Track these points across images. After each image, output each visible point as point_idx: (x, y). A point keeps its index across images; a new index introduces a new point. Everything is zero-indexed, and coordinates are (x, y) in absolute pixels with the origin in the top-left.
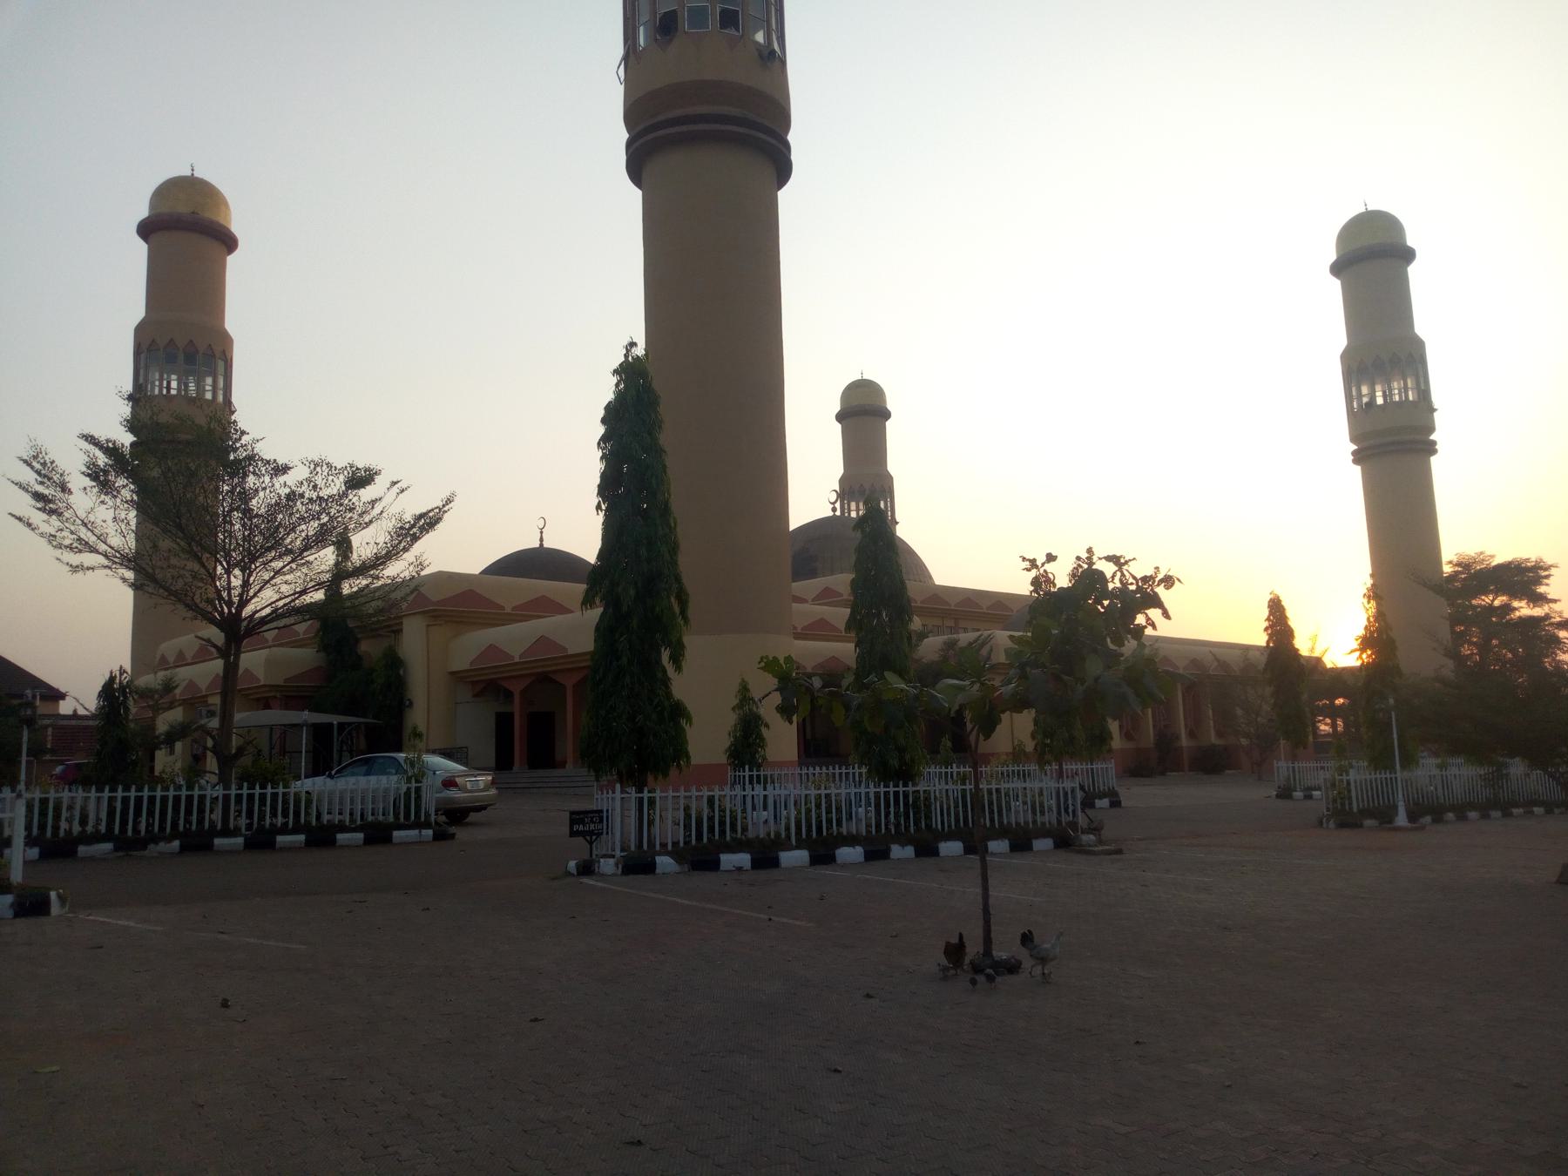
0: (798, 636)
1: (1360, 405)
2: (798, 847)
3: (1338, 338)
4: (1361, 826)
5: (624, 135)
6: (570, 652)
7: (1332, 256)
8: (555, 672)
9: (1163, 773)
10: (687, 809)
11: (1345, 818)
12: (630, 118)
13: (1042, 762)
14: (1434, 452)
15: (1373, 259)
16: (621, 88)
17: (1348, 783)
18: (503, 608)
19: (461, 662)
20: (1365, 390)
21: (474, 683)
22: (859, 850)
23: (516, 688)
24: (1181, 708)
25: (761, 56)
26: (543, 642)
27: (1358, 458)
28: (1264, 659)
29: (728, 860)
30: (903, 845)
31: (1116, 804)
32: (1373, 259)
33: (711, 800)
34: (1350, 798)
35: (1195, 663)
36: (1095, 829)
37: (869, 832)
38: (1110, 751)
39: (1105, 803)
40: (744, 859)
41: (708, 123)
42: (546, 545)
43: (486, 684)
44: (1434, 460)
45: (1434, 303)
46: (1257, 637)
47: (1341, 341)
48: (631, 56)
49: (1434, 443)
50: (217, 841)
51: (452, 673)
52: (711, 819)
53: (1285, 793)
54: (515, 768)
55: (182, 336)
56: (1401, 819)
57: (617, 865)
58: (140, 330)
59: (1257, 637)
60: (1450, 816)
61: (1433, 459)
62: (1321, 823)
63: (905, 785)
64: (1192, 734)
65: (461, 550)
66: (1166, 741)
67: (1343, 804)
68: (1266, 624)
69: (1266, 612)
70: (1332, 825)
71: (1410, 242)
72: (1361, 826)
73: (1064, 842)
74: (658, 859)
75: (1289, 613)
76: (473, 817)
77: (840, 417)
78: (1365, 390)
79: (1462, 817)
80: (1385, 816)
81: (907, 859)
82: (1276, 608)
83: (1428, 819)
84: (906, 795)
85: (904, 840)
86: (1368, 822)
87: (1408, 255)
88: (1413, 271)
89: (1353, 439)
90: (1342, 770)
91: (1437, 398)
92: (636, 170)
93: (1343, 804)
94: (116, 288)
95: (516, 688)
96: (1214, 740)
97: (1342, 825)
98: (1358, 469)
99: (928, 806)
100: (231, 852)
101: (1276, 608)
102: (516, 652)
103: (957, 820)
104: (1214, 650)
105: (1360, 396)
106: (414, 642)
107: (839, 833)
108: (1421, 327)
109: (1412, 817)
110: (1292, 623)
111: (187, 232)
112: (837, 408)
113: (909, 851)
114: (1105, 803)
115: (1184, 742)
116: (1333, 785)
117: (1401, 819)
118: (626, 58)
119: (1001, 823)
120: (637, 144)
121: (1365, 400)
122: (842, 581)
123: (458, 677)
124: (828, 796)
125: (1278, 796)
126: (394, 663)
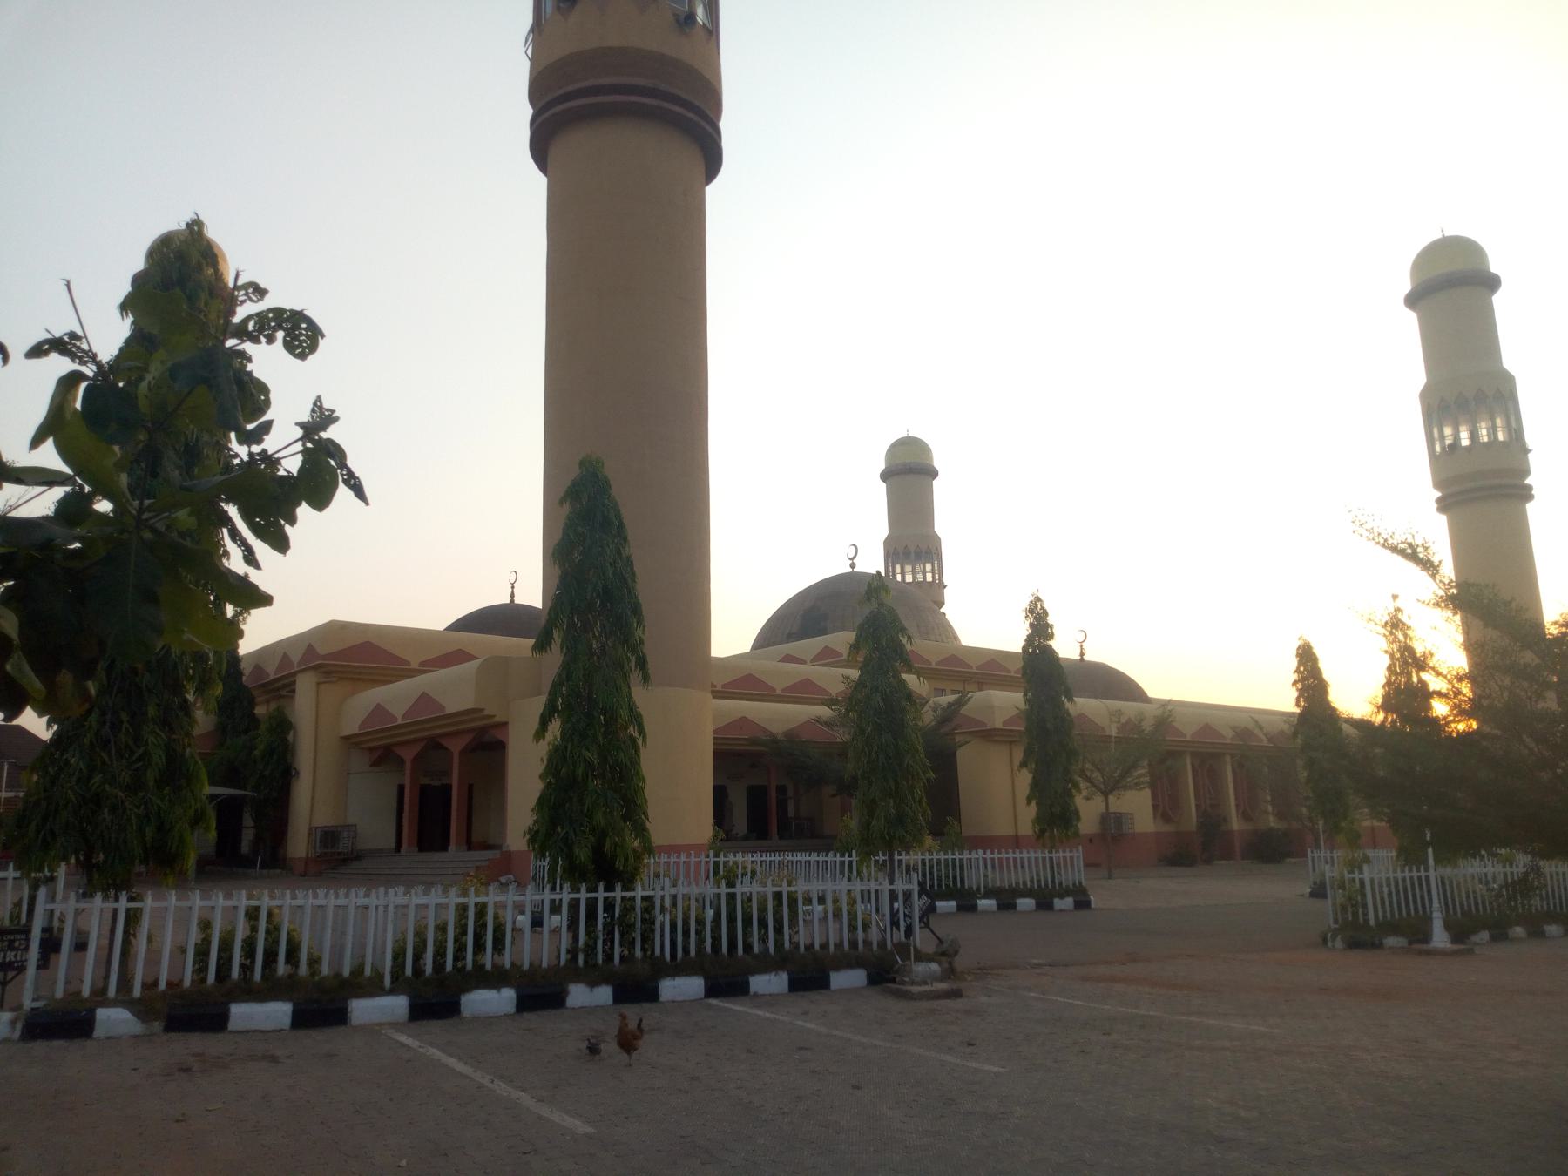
0: (717, 694)
1: (1443, 447)
2: (392, 992)
3: (1418, 376)
4: (1380, 946)
5: (528, 112)
6: (448, 711)
7: (1406, 286)
8: (441, 736)
9: (1208, 861)
10: (206, 926)
11: (1359, 935)
12: (534, 96)
13: (866, 855)
14: (1529, 497)
15: (1453, 287)
16: (527, 64)
17: (1362, 882)
18: (408, 663)
19: (351, 727)
20: (1448, 431)
21: (371, 750)
22: (509, 994)
23: (408, 754)
24: (1231, 786)
25: (678, 21)
26: (424, 699)
27: (1444, 505)
28: (1020, 664)
30: (593, 984)
31: (1082, 904)
32: (1453, 287)
33: (252, 914)
34: (1365, 906)
35: (1207, 729)
36: (945, 954)
38: (1077, 834)
39: (1068, 902)
40: (278, 1012)
41: (626, 102)
42: (517, 601)
43: (379, 749)
44: (1530, 507)
45: (1521, 332)
46: (1283, 699)
48: (538, 28)
49: (1530, 488)
51: (347, 738)
52: (249, 946)
53: (1319, 892)
54: (452, 847)
56: (1440, 938)
57: (13, 1023)
58: (1426, 395)
59: (1283, 699)
60: (1519, 931)
62: (1325, 941)
63: (609, 888)
64: (1246, 816)
65: (1023, 706)
66: (1211, 825)
67: (1355, 914)
68: (1295, 677)
69: (1293, 663)
70: (1339, 944)
71: (1494, 268)
72: (1380, 946)
73: (883, 973)
74: (102, 1014)
75: (1322, 665)
76: (56, 924)
77: (885, 476)
78: (1448, 431)
79: (1536, 933)
80: (1418, 933)
82: (1306, 657)
83: (1484, 936)
84: (609, 905)
85: (593, 978)
86: (1391, 941)
88: (1499, 300)
89: (1438, 484)
90: (1355, 865)
91: (1530, 438)
92: (541, 150)
93: (1355, 914)
96: (1273, 822)
97: (1353, 944)
98: (1443, 518)
99: (649, 922)
101: (1306, 657)
102: (398, 711)
103: (716, 940)
104: (1256, 716)
105: (1442, 437)
106: (305, 705)
107: (478, 967)
108: (1510, 361)
109: (1460, 932)
110: (1326, 676)
112: (882, 466)
113: (604, 994)
114: (1068, 902)
115: (1236, 824)
116: (1342, 886)
117: (1440, 938)
118: (532, 30)
119: (779, 944)
120: (540, 119)
121: (1448, 441)
122: (841, 640)
123: (350, 741)
124: (687, 897)
125: (1312, 895)
126: (282, 726)
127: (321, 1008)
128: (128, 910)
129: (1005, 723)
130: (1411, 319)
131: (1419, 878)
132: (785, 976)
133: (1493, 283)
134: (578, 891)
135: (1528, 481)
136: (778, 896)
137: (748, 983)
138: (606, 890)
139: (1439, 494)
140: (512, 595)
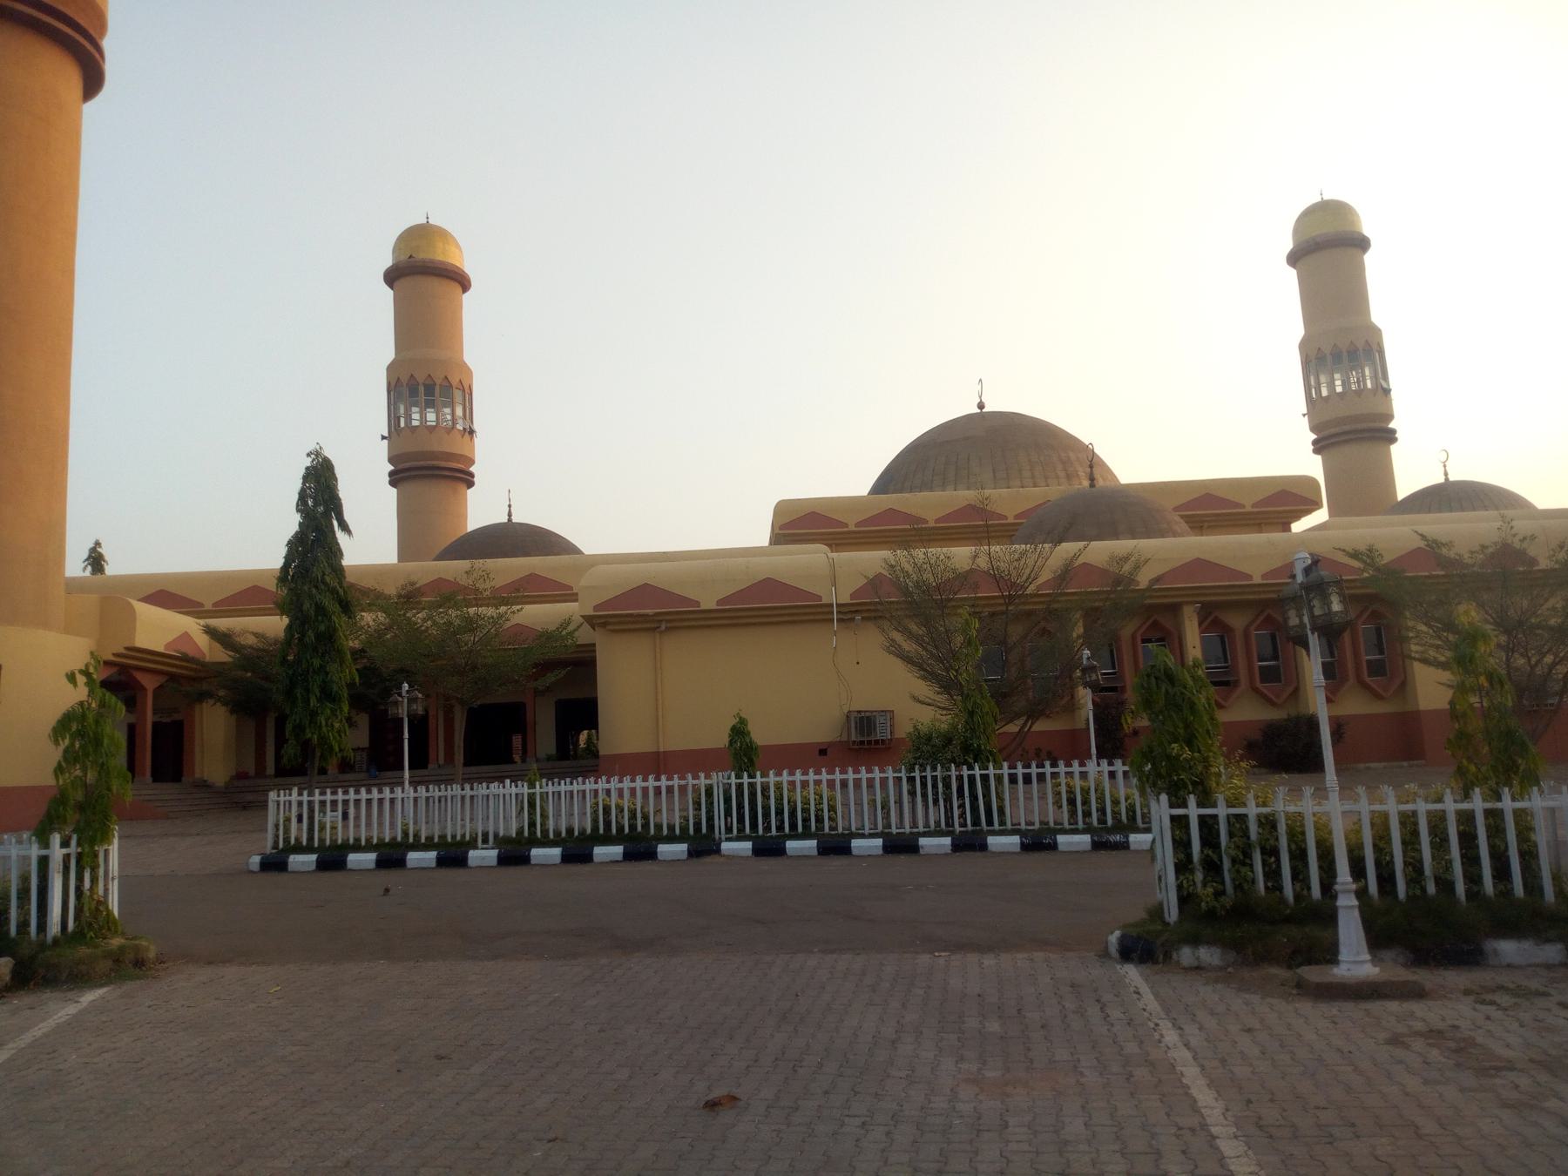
3: (1296, 329)
7: (1288, 245)
15: (1328, 250)
29: (414, 857)
32: (1328, 250)
37: (633, 827)
40: (617, 851)
45: (1390, 294)
47: (1298, 330)
49: (1393, 432)
50: (535, 852)
55: (425, 381)
58: (1304, 346)
61: (1393, 448)
81: (875, 852)
87: (1362, 244)
88: (1369, 258)
89: (1313, 429)
94: (370, 332)
95: (149, 683)
98: (1319, 458)
100: (1076, 854)
111: (423, 275)
127: (640, 848)
128: (1201, 817)
129: (852, 596)
130: (1292, 274)
131: (1466, 818)
133: (1362, 244)
134: (1184, 805)
135: (1391, 425)
136: (1437, 824)
138: (1200, 805)
140: (510, 515)
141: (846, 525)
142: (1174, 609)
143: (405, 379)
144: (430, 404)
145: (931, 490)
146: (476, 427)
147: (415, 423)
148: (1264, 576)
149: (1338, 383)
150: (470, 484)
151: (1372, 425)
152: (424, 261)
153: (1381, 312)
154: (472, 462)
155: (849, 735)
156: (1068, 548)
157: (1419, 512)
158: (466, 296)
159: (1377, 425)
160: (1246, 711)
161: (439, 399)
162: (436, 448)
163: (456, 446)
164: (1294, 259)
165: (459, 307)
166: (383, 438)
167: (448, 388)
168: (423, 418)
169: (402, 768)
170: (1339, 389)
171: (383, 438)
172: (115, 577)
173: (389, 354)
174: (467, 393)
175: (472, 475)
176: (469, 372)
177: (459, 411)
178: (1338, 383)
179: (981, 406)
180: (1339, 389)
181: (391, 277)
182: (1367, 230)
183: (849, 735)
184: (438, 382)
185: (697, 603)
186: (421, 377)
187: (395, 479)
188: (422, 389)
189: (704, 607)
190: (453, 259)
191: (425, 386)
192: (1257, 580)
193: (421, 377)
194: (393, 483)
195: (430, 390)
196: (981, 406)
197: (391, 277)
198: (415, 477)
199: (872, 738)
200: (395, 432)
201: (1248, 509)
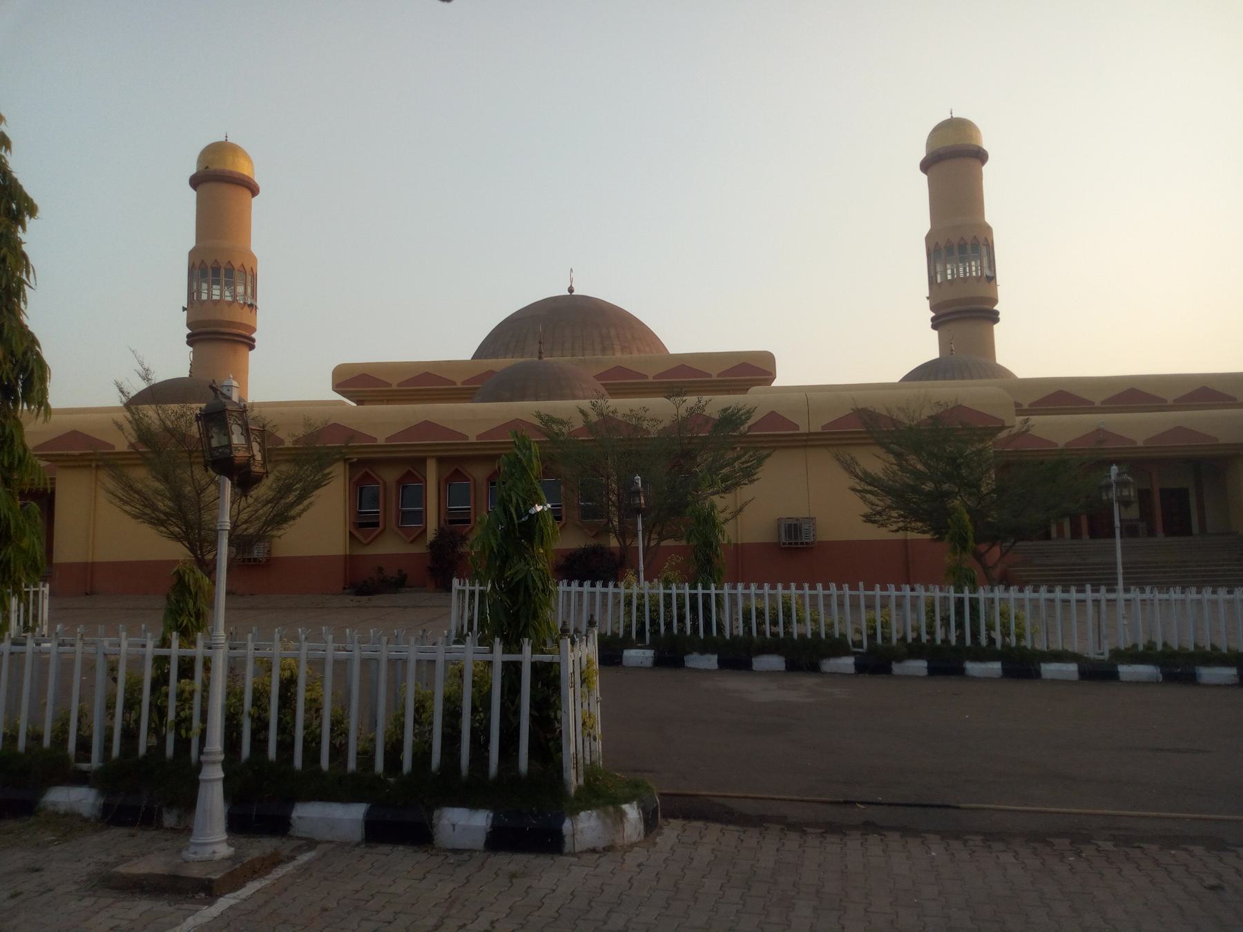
6: (1221, 442)
7: (922, 154)
15: (954, 159)
32: (954, 159)
47: (925, 226)
49: (997, 313)
61: (996, 326)
88: (987, 169)
89: (932, 308)
94: (911, 208)
98: (936, 333)
132: (715, 658)
135: (996, 308)
137: (621, 657)
139: (189, 331)
141: (454, 383)
142: (423, 461)
143: (197, 264)
144: (963, 260)
145: (497, 357)
146: (259, 304)
147: (215, 298)
148: (478, 437)
149: (949, 272)
150: (252, 347)
151: (974, 306)
152: (231, 172)
153: (993, 213)
154: (254, 330)
155: (779, 536)
156: (691, 400)
157: (928, 379)
158: (255, 200)
159: (986, 307)
160: (569, 541)
161: (223, 279)
162: (238, 320)
163: (242, 316)
164: (926, 166)
165: (250, 207)
166: (184, 309)
167: (230, 272)
168: (210, 294)
169: (1112, 535)
170: (949, 277)
171: (184, 309)
172: (1062, 396)
173: (191, 243)
174: (251, 277)
175: (254, 340)
176: (255, 260)
177: (240, 289)
178: (949, 272)
179: (571, 290)
180: (949, 277)
181: (195, 182)
182: (986, 145)
183: (779, 536)
184: (223, 265)
185: (113, 447)
186: (209, 263)
187: (192, 340)
188: (210, 272)
189: (117, 450)
190: (243, 169)
191: (213, 269)
192: (473, 439)
193: (209, 263)
194: (190, 343)
195: (216, 271)
196: (571, 290)
197: (195, 182)
198: (210, 340)
199: (799, 541)
200: (193, 303)
201: (714, 378)
